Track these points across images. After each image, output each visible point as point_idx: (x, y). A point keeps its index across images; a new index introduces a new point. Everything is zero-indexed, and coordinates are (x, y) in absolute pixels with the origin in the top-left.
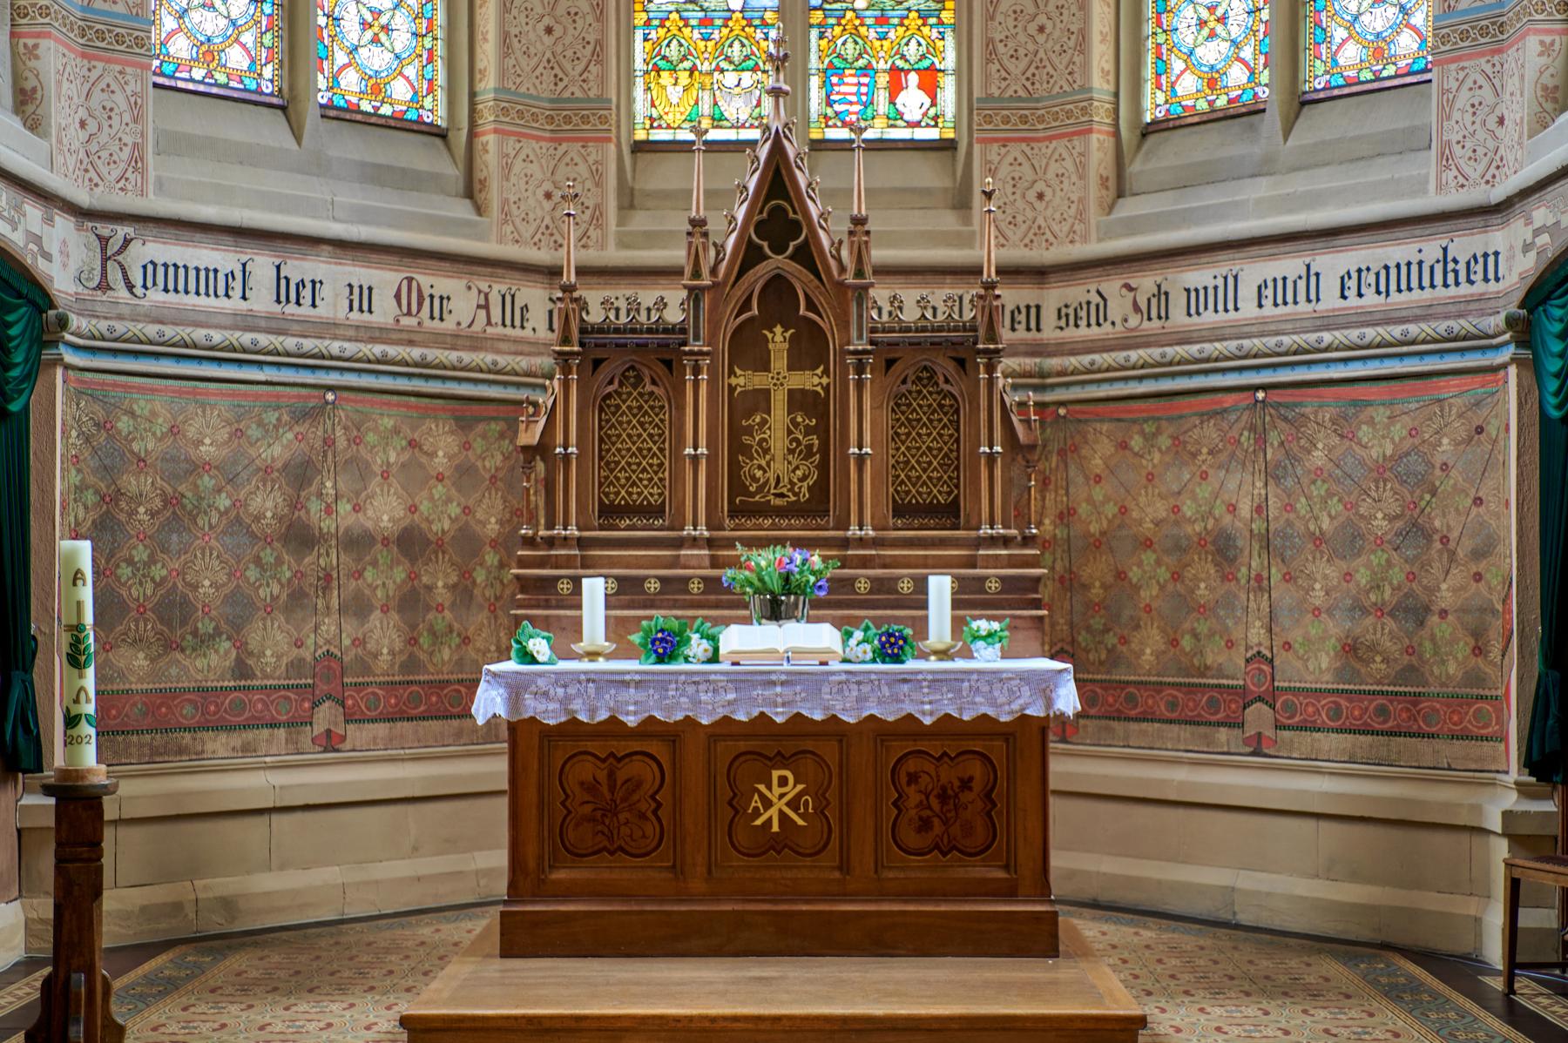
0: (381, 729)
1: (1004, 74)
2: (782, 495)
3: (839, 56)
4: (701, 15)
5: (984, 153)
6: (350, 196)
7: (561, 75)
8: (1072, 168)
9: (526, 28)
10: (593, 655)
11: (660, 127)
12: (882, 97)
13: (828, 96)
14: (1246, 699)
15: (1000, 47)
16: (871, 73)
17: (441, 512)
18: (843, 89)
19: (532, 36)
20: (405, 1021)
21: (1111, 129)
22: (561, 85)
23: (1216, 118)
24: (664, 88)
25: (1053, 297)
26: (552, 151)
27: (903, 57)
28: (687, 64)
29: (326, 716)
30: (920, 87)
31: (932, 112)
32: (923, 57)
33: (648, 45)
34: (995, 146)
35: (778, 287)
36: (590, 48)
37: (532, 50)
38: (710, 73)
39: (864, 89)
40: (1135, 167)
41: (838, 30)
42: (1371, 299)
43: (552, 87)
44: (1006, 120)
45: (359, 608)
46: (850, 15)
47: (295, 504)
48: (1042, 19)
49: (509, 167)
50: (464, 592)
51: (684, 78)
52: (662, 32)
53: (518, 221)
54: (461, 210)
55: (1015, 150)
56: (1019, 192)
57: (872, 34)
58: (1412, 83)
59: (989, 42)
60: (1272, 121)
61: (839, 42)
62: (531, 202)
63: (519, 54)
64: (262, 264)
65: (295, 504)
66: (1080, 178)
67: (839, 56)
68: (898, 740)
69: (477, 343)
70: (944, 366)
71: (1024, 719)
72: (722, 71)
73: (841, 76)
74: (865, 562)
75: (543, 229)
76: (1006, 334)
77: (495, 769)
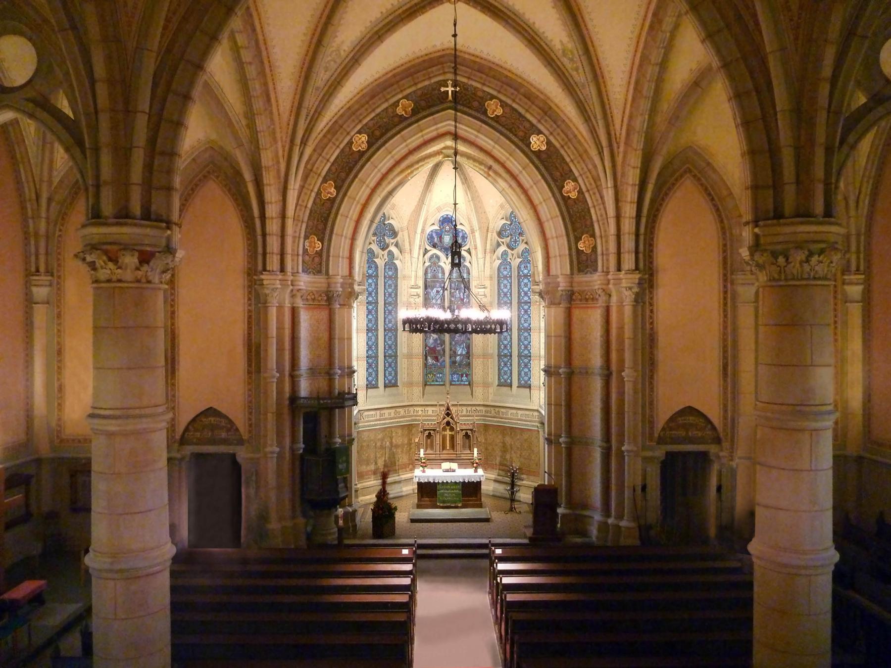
35: (448, 423)
50: (402, 452)
64: (378, 412)
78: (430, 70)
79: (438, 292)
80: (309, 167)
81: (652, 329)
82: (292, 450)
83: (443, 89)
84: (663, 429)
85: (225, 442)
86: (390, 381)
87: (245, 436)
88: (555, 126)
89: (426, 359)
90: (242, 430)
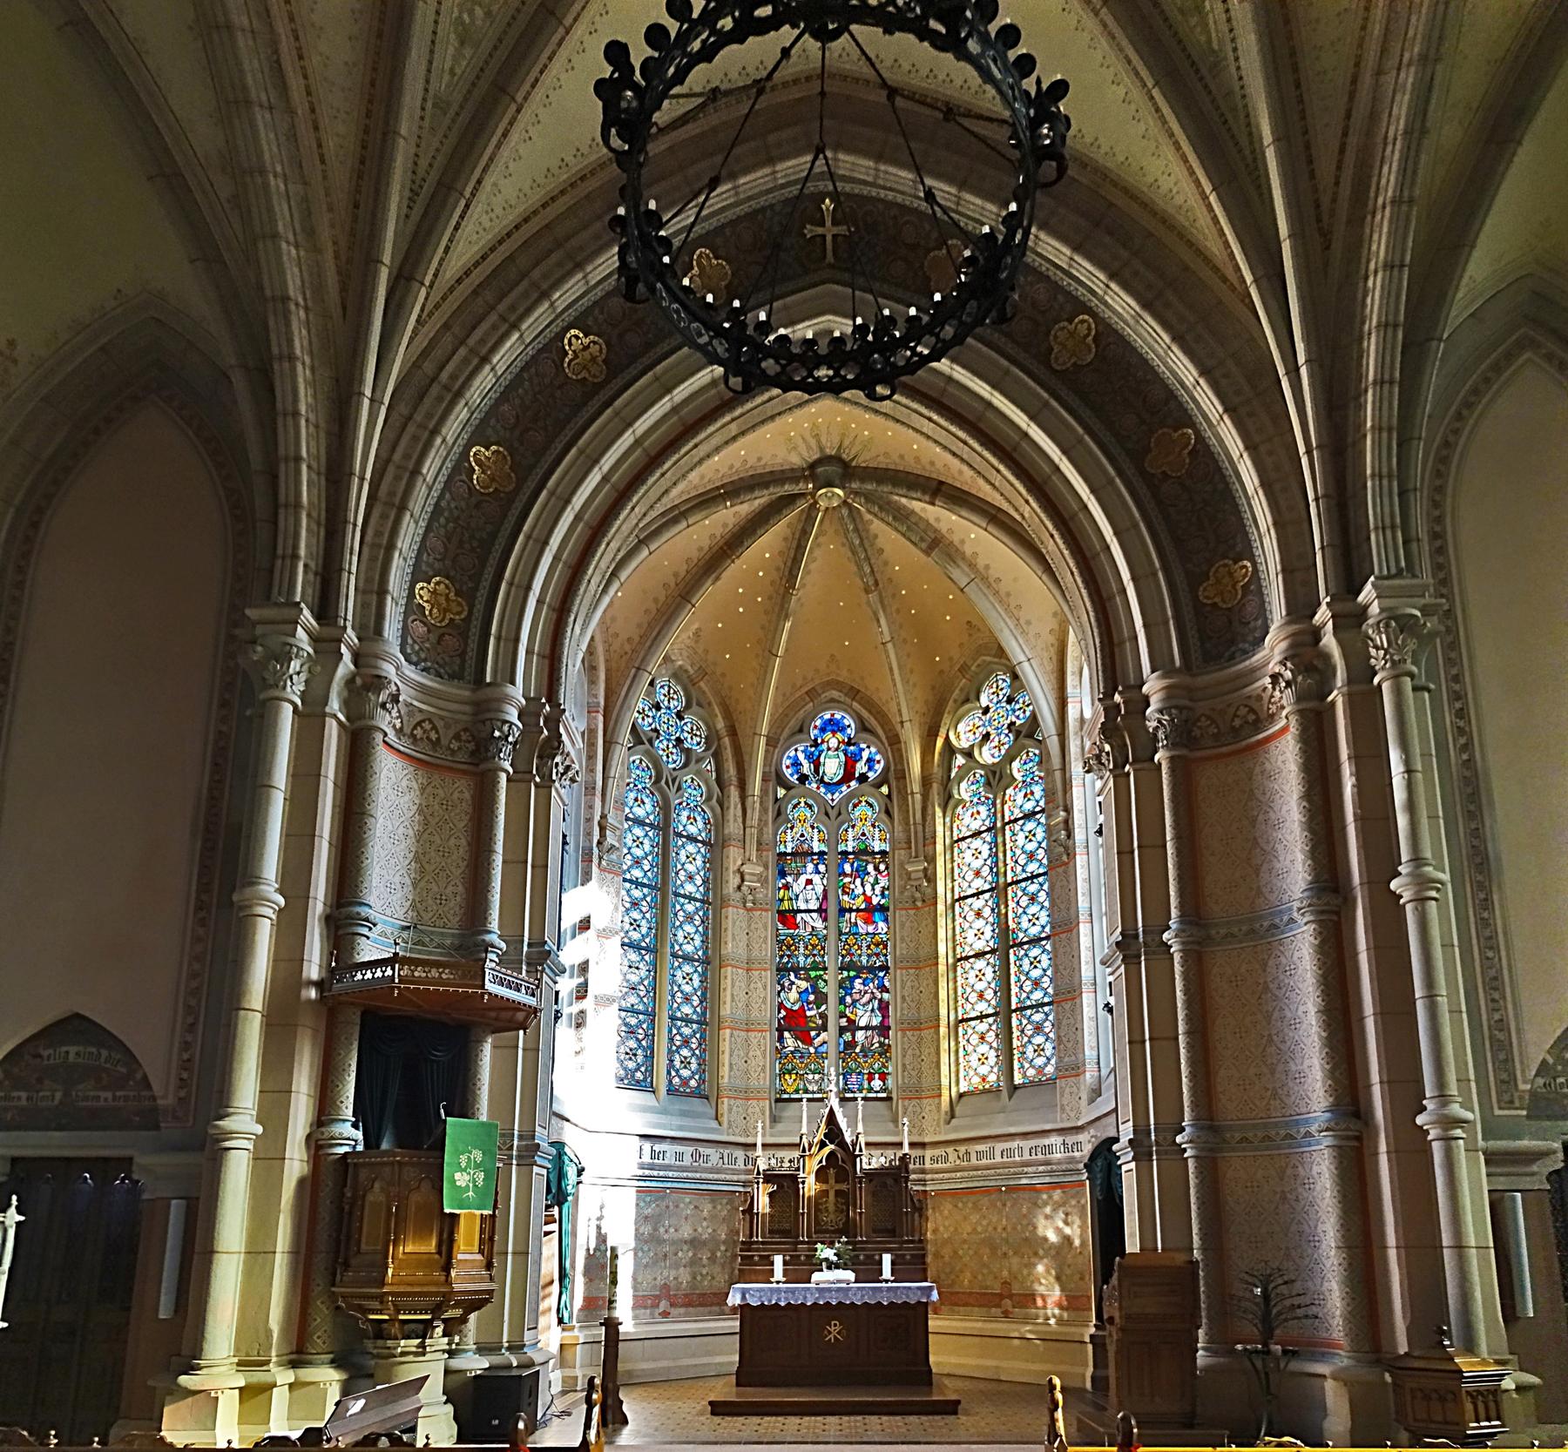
0: (682, 1310)
2: (570, 344)
6: (677, 1121)
10: (887, 1281)
14: (1001, 1296)
17: (705, 1231)
20: (711, 1403)
23: (985, 1091)
25: (929, 1153)
29: (663, 1305)
40: (958, 1110)
42: (1040, 1156)
45: (676, 1266)
47: (655, 1229)
50: (713, 1259)
54: (714, 1124)
55: (914, 1102)
58: (1052, 1081)
60: (1005, 1094)
65: (655, 1229)
68: (873, 1310)
69: (718, 1171)
70: (890, 1181)
71: (919, 1302)
74: (863, 1249)
76: (911, 1166)
77: (735, 1325)
78: (772, 138)
79: (809, 882)
80: (428, 367)
81: (1469, 764)
82: (317, 1144)
83: (810, 230)
84: (1543, 1068)
85: (94, 1119)
86: (685, 1082)
87: (167, 1101)
88: (1125, 254)
89: (781, 1039)
90: (157, 1088)
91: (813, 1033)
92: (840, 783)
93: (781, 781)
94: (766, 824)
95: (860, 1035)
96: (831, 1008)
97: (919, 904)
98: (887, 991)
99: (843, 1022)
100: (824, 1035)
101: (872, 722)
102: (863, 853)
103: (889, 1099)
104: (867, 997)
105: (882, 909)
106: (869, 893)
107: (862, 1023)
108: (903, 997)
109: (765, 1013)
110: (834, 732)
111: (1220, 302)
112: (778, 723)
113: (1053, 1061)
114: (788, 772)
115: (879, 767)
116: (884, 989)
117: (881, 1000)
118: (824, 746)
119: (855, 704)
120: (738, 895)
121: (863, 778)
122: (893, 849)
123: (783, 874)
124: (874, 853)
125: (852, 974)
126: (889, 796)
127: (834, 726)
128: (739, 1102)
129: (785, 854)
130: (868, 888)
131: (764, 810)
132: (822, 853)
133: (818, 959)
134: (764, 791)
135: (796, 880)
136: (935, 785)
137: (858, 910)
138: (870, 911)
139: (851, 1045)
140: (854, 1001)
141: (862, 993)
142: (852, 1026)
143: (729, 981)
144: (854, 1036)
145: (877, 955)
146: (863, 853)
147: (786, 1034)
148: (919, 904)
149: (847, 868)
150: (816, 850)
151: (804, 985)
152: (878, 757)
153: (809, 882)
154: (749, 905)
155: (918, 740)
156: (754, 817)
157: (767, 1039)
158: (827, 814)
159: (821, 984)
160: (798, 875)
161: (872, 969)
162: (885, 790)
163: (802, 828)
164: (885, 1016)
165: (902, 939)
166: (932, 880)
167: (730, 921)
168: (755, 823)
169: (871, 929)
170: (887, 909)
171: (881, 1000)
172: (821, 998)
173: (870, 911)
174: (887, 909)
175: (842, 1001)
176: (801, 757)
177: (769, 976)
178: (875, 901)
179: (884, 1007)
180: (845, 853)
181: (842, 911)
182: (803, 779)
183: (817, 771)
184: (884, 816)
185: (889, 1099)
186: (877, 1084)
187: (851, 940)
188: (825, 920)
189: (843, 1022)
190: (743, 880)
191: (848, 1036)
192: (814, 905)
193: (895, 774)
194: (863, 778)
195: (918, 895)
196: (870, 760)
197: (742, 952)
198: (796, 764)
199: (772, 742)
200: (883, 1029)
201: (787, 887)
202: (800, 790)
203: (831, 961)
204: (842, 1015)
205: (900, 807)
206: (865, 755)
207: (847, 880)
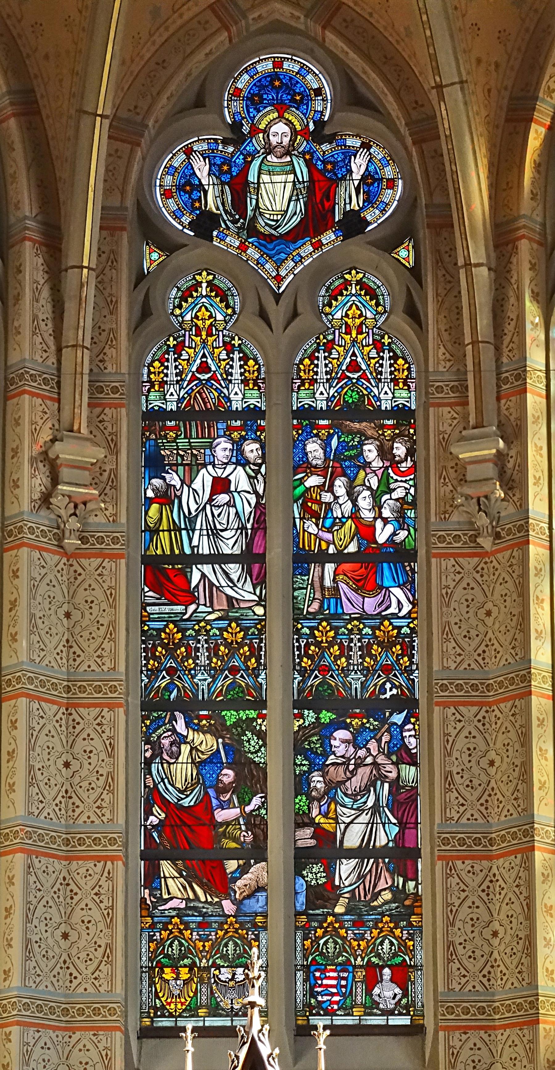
1: (459, 651)
3: (321, 954)
4: (199, 919)
5: (447, 1040)
7: (75, 974)
8: (523, 1053)
9: (45, 935)
11: (163, 1016)
12: (360, 989)
13: (312, 988)
15: (457, 778)
16: (351, 969)
18: (325, 982)
19: (50, 941)
21: (548, 544)
22: (75, 982)
24: (167, 981)
26: (67, 1039)
27: (378, 956)
28: (186, 961)
30: (392, 980)
31: (404, 1001)
32: (395, 955)
33: (152, 946)
34: (457, 1033)
36: (101, 951)
37: (51, 954)
38: (207, 969)
39: (343, 983)
41: (320, 932)
43: (68, 984)
44: (466, 1011)
46: (330, 919)
48: (489, 606)
49: (29, 1054)
51: (184, 974)
52: (165, 934)
53: (42, 785)
55: (474, 1037)
56: (474, 760)
57: (350, 935)
59: (450, 944)
61: (322, 942)
62: (53, 769)
63: (39, 957)
66: (530, 1062)
67: (321, 954)
72: (218, 967)
73: (324, 971)
75: (63, 793)
79: (221, 485)
89: (152, 877)
91: (232, 865)
92: (295, 236)
93: (151, 229)
94: (113, 335)
95: (346, 869)
96: (275, 803)
97: (486, 543)
98: (413, 762)
99: (305, 837)
100: (257, 871)
101: (374, 82)
102: (353, 412)
103: (415, 1030)
104: (364, 773)
105: (400, 555)
106: (367, 515)
107: (353, 839)
108: (448, 777)
109: (119, 817)
110: (281, 108)
111: (101, 228)
112: (141, 81)
113: (273, 232)
114: (167, 208)
115: (392, 197)
116: (406, 757)
117: (395, 784)
118: (258, 142)
119: (330, 36)
120: (44, 519)
121: (353, 225)
122: (426, 405)
123: (156, 465)
124: (378, 414)
125: (326, 717)
126: (416, 272)
127: (281, 92)
128: (47, 1036)
129: (163, 414)
130: (365, 501)
131: (107, 303)
132: (252, 415)
133: (243, 680)
134: (107, 257)
135: (187, 481)
136: (524, 245)
137: (340, 558)
138: (370, 563)
139: (323, 895)
140: (332, 786)
141: (351, 765)
142: (327, 848)
143: (21, 733)
144: (330, 872)
145: (387, 669)
146: (353, 412)
147: (167, 868)
148: (486, 543)
149: (314, 449)
150: (237, 405)
151: (207, 743)
152: (389, 172)
153: (221, 485)
154: (72, 542)
155: (480, 129)
156: (83, 321)
157: (123, 877)
158: (263, 315)
159: (251, 742)
160: (193, 468)
161: (375, 707)
162: (405, 254)
163: (206, 343)
164: (407, 823)
165: (447, 632)
166: (513, 479)
167: (23, 583)
168: (86, 335)
169: (370, 604)
170: (412, 555)
171: (395, 784)
172: (252, 779)
173: (370, 563)
174: (412, 555)
175: (301, 785)
176: (202, 169)
177: (122, 723)
178: (383, 534)
179: (404, 802)
180: (307, 415)
181: (303, 559)
182: (205, 224)
183: (239, 203)
184: (401, 322)
185: (415, 1030)
186: (387, 991)
187: (325, 633)
188: (260, 581)
189: (305, 837)
190: (55, 480)
191: (315, 874)
192: (230, 544)
193: (429, 216)
194: (353, 225)
195: (482, 520)
196: (370, 179)
197: (54, 664)
198: (189, 186)
199: (125, 132)
200: (402, 857)
201: (166, 498)
202: (198, 252)
203: (277, 682)
204: (303, 820)
205: (440, 304)
206: (359, 166)
207: (313, 481)
